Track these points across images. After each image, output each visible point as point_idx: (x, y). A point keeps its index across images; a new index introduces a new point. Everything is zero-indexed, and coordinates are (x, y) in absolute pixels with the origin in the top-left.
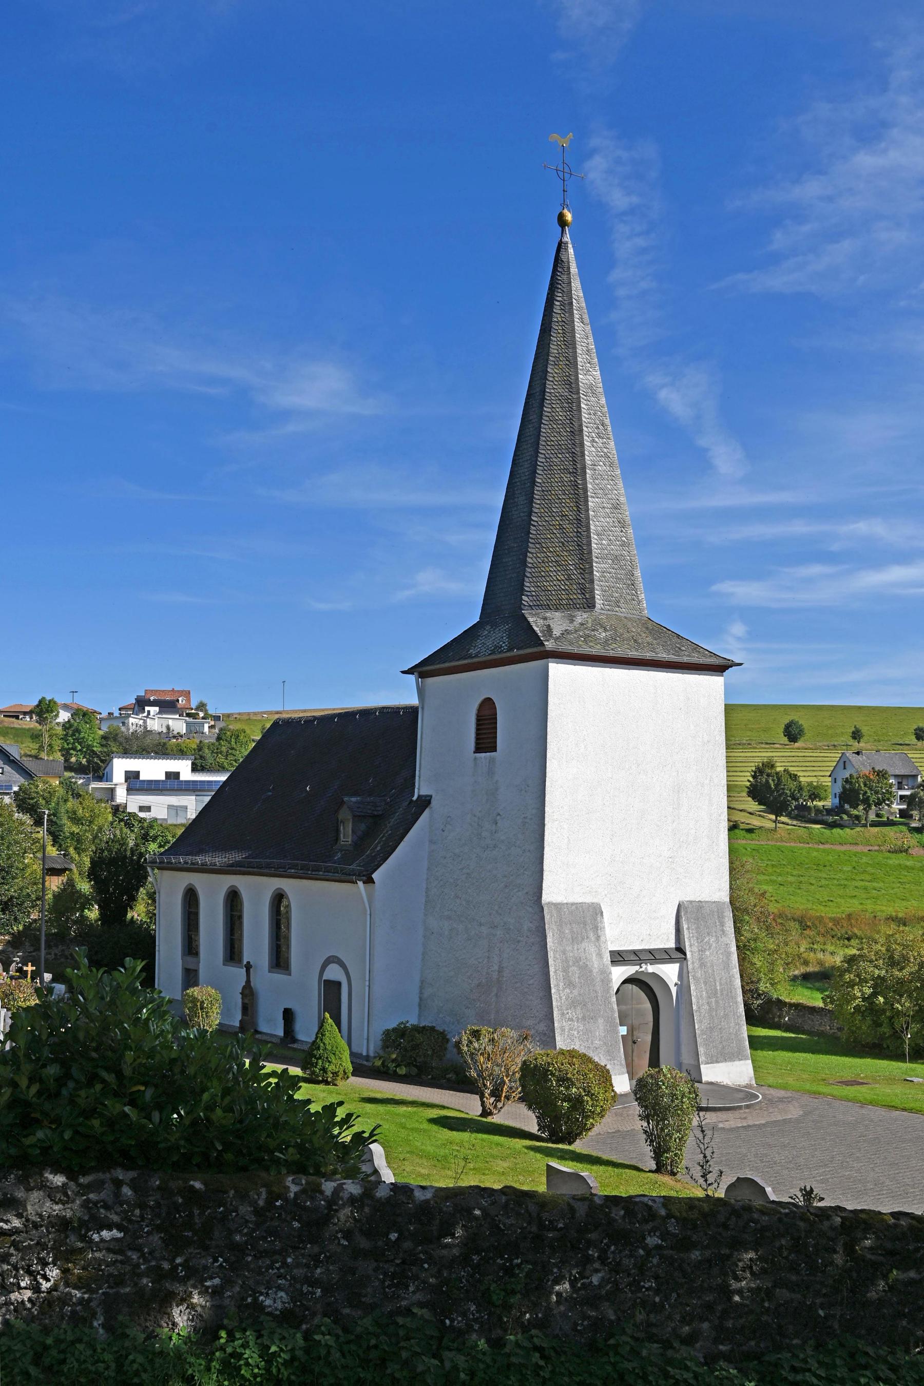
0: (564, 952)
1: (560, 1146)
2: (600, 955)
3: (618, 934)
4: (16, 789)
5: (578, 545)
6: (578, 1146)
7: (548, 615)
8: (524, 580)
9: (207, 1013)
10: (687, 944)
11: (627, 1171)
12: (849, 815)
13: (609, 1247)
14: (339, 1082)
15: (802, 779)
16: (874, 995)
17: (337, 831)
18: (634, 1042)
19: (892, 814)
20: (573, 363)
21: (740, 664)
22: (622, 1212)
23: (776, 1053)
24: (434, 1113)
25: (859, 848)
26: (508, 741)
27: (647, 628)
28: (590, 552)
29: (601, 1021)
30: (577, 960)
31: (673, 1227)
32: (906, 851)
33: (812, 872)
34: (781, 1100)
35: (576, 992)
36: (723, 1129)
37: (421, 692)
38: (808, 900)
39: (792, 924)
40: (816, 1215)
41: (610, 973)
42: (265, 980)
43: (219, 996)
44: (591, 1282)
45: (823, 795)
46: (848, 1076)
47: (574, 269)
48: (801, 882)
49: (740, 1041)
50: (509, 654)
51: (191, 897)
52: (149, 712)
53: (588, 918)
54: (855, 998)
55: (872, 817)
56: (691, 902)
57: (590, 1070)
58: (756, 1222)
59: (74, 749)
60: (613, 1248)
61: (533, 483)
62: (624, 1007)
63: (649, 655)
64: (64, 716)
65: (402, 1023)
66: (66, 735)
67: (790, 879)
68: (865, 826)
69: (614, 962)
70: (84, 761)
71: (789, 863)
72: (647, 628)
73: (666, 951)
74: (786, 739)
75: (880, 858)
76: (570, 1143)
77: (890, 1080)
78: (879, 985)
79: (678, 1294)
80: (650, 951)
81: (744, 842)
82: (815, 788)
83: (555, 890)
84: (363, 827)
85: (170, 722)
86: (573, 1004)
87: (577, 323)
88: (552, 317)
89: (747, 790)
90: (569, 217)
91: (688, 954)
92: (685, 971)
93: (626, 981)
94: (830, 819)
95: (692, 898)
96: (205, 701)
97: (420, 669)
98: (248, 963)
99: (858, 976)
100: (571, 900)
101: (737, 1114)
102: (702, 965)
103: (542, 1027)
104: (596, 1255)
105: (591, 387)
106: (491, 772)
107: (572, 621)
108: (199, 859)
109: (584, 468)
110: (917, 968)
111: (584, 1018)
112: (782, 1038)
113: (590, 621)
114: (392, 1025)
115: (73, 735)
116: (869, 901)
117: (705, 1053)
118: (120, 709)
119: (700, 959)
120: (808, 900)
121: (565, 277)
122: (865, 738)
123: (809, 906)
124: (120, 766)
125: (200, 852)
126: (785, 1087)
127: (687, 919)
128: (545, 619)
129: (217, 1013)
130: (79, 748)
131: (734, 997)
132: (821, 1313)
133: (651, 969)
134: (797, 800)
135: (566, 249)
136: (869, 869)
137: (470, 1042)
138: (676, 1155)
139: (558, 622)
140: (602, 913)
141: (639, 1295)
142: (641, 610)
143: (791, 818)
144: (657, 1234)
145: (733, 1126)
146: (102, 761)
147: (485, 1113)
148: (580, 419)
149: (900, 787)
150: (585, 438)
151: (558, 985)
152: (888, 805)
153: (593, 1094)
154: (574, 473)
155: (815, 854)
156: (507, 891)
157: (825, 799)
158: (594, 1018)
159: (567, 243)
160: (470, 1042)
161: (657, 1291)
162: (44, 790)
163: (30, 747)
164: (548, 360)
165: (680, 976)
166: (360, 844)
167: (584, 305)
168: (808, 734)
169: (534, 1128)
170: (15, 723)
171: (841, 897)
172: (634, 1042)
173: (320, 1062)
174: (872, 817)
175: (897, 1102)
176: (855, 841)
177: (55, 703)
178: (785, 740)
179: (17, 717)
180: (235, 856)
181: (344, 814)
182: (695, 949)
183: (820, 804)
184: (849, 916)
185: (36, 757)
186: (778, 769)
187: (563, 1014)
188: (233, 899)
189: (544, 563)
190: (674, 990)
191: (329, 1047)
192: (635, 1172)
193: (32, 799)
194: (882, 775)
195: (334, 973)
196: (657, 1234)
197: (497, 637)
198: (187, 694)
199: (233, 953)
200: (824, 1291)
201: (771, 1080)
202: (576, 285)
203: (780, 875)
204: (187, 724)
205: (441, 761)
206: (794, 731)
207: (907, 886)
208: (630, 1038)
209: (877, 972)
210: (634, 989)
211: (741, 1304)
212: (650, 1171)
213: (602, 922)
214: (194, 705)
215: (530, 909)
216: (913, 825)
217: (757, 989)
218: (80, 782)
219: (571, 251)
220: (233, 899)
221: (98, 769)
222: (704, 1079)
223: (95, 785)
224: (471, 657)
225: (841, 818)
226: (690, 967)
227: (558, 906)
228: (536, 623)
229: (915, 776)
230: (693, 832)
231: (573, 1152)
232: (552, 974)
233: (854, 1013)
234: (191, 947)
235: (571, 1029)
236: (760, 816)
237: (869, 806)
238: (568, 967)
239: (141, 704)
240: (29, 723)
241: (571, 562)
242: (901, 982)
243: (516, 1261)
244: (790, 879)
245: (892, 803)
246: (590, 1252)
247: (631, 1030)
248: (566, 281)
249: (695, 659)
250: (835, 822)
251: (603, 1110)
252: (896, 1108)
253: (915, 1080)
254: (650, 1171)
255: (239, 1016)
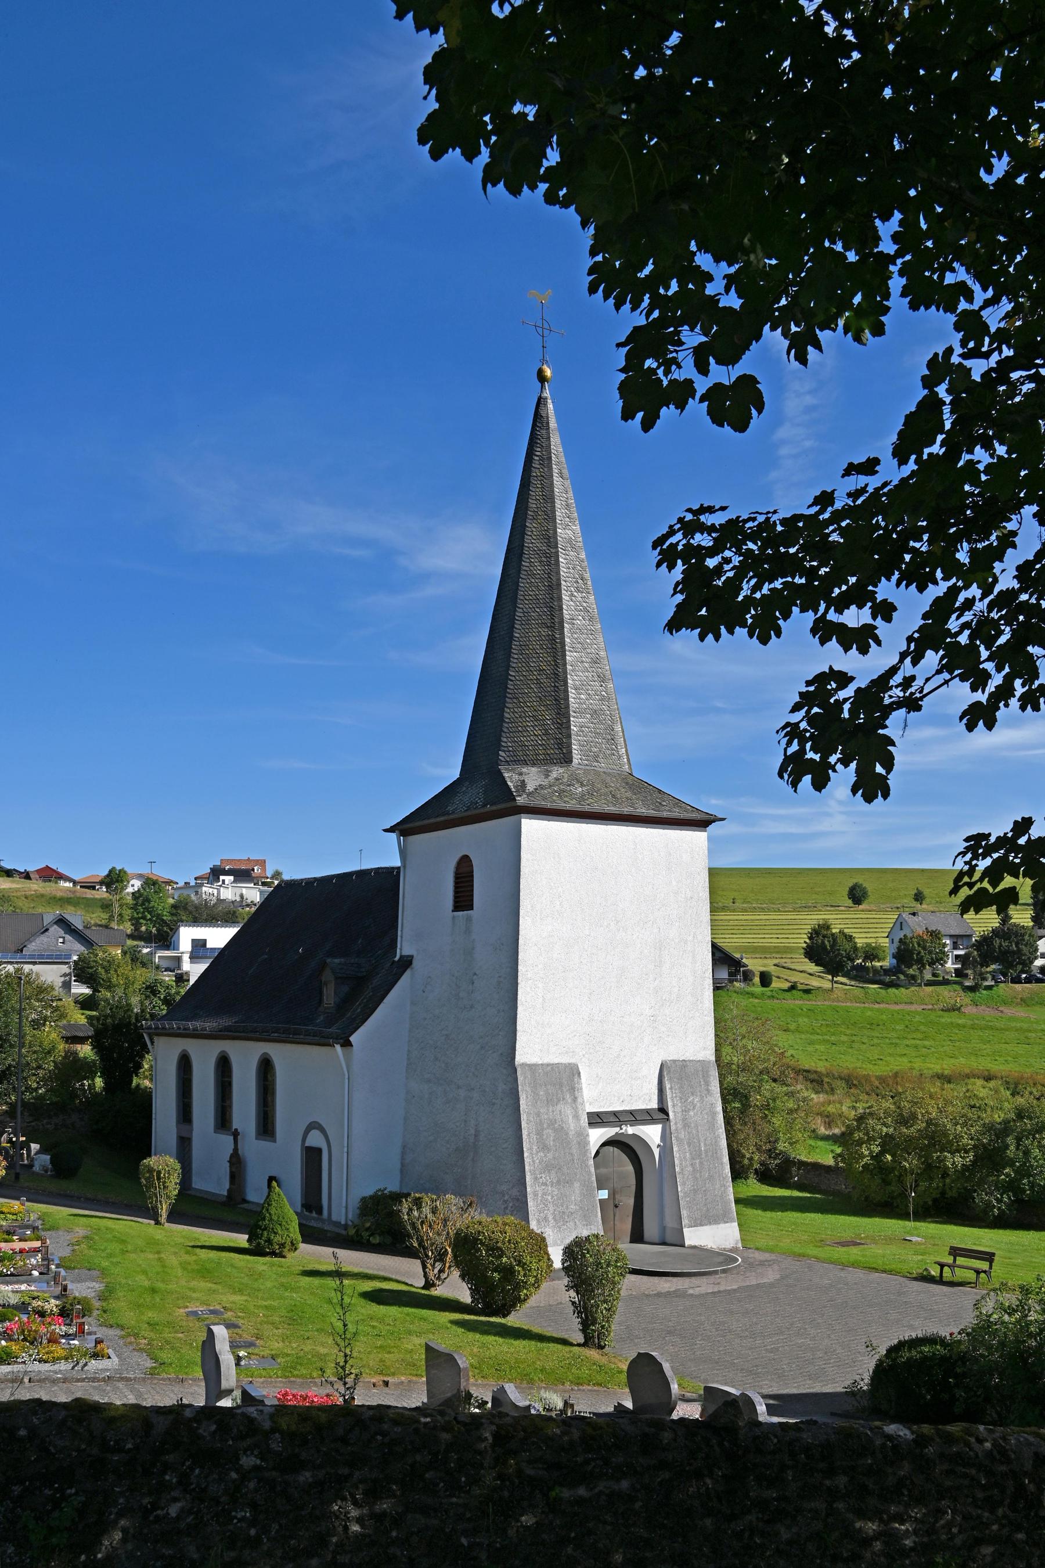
0: (538, 1115)
1: (493, 1319)
2: (576, 1117)
3: (595, 1096)
4: (75, 958)
5: (556, 700)
6: (513, 1320)
7: (524, 770)
8: (501, 736)
9: (164, 1182)
10: (670, 1104)
11: (551, 1345)
12: (906, 975)
13: (192, 1470)
14: (286, 1252)
15: (857, 940)
16: (882, 1153)
17: (321, 993)
18: (616, 1206)
19: (947, 973)
20: (551, 517)
21: (723, 819)
22: (214, 1427)
23: (786, 1214)
24: (368, 1286)
25: (913, 1008)
26: (483, 896)
27: (627, 783)
28: (567, 706)
29: (577, 1185)
30: (552, 1123)
31: (276, 1444)
32: (959, 1009)
33: (865, 1032)
34: (762, 1263)
35: (550, 1155)
36: (692, 1295)
37: (403, 853)
38: (858, 1059)
39: (839, 1082)
40: (465, 1424)
41: (588, 1135)
42: (252, 1147)
43: (178, 1166)
44: (168, 1514)
45: (881, 955)
46: (848, 1235)
47: (553, 424)
48: (853, 1041)
49: (727, 1203)
50: (482, 810)
51: (185, 1064)
52: (224, 881)
53: (564, 1079)
54: (865, 1156)
55: (928, 976)
56: (674, 1061)
57: (523, 1239)
58: (384, 1434)
59: (144, 918)
60: (197, 1471)
61: (511, 637)
62: (603, 1171)
63: (626, 810)
64: (136, 885)
65: (380, 1190)
66: (136, 904)
67: (844, 1038)
68: (920, 985)
69: (592, 1124)
70: (154, 930)
71: (844, 1023)
72: (627, 783)
73: (648, 1112)
74: (850, 901)
75: (932, 1016)
76: (504, 1316)
77: (889, 1240)
78: (888, 1143)
79: (280, 1525)
80: (631, 1112)
81: (745, 998)
82: (874, 948)
83: (531, 1049)
84: (345, 989)
85: (244, 891)
86: (548, 1168)
87: (556, 479)
88: (531, 471)
89: (803, 951)
90: (548, 373)
91: (671, 1114)
92: (668, 1131)
93: (604, 1145)
94: (887, 979)
95: (675, 1058)
96: (280, 870)
97: (401, 827)
98: (236, 1130)
99: (867, 1134)
100: (546, 1061)
101: (712, 1279)
102: (686, 1125)
103: (515, 1192)
104: (174, 1480)
105: (570, 541)
106: (468, 931)
107: (547, 776)
108: (190, 1025)
109: (561, 622)
110: (924, 1125)
111: (558, 1182)
112: (801, 1198)
113: (566, 776)
114: (370, 1192)
115: (143, 904)
116: (918, 1059)
117: (689, 1216)
118: (196, 879)
119: (684, 1119)
120: (858, 1059)
121: (544, 432)
122: (928, 900)
123: (859, 1065)
124: (187, 935)
125: (194, 1017)
126: (771, 1251)
127: (670, 1079)
128: (521, 774)
129: (176, 1184)
130: (149, 917)
131: (719, 1159)
132: (464, 1541)
133: (630, 1130)
134: (853, 961)
135: (546, 405)
136: (922, 1028)
137: (411, 1210)
138: (603, 1327)
139: (533, 777)
140: (579, 1074)
141: (231, 1527)
142: (621, 765)
143: (850, 978)
144: (256, 1452)
145: (703, 1292)
146: (171, 930)
147: (429, 1285)
148: (558, 573)
149: (955, 947)
150: (563, 592)
151: (531, 1149)
152: (942, 965)
153: (525, 1264)
154: (552, 627)
155: (869, 1013)
156: (483, 1052)
157: (884, 959)
158: (569, 1182)
159: (546, 398)
160: (411, 1210)
161: (253, 1523)
162: (103, 959)
163: (98, 917)
164: (526, 514)
165: (663, 1137)
166: (344, 1003)
167: (563, 460)
168: (872, 897)
169: (468, 1300)
170: (89, 894)
171: (890, 1055)
172: (616, 1206)
173: (265, 1233)
174: (928, 976)
175: (879, 1263)
176: (912, 1001)
177: (125, 872)
178: (850, 903)
179: (94, 888)
180: (226, 1022)
181: (328, 976)
182: (678, 1109)
183: (878, 964)
184: (896, 1075)
185: (106, 927)
186: (834, 931)
187: (536, 1179)
188: (224, 1065)
189: (523, 720)
190: (656, 1152)
191: (275, 1218)
192: (560, 1346)
193: (92, 968)
194: (935, 935)
195: (315, 1139)
196: (256, 1452)
197: (474, 794)
198: (262, 863)
199: (223, 1120)
200: (468, 1515)
201: (762, 1243)
202: (555, 440)
203: (833, 1034)
204: (261, 892)
205: (422, 922)
206: (858, 893)
207: (958, 1044)
208: (612, 1202)
209: (885, 1129)
210: (610, 1149)
211: (362, 1535)
212: (579, 1345)
213: (579, 1083)
214: (269, 874)
215: (505, 1071)
216: (967, 983)
217: (775, 1149)
218: (145, 951)
219: (550, 406)
220: (224, 1065)
221: (166, 939)
222: (687, 1243)
223: (160, 953)
224: (448, 814)
225: (898, 978)
226: (673, 1128)
227: (532, 1067)
228: (511, 778)
229: (970, 936)
230: (676, 990)
231: (503, 1326)
232: (525, 1137)
233: (862, 1172)
234: (185, 1114)
235: (544, 1194)
236: (819, 976)
237: (924, 966)
238: (543, 1129)
239: (216, 873)
240: (102, 892)
241: (548, 716)
242: (909, 1139)
243: (69, 1491)
244: (844, 1038)
245: (946, 962)
246: (167, 1477)
247: (613, 1194)
248: (545, 436)
249: (677, 814)
250: (892, 982)
251: (537, 1281)
252: (875, 1270)
253: (914, 1239)
254: (579, 1345)
255: (227, 1185)
